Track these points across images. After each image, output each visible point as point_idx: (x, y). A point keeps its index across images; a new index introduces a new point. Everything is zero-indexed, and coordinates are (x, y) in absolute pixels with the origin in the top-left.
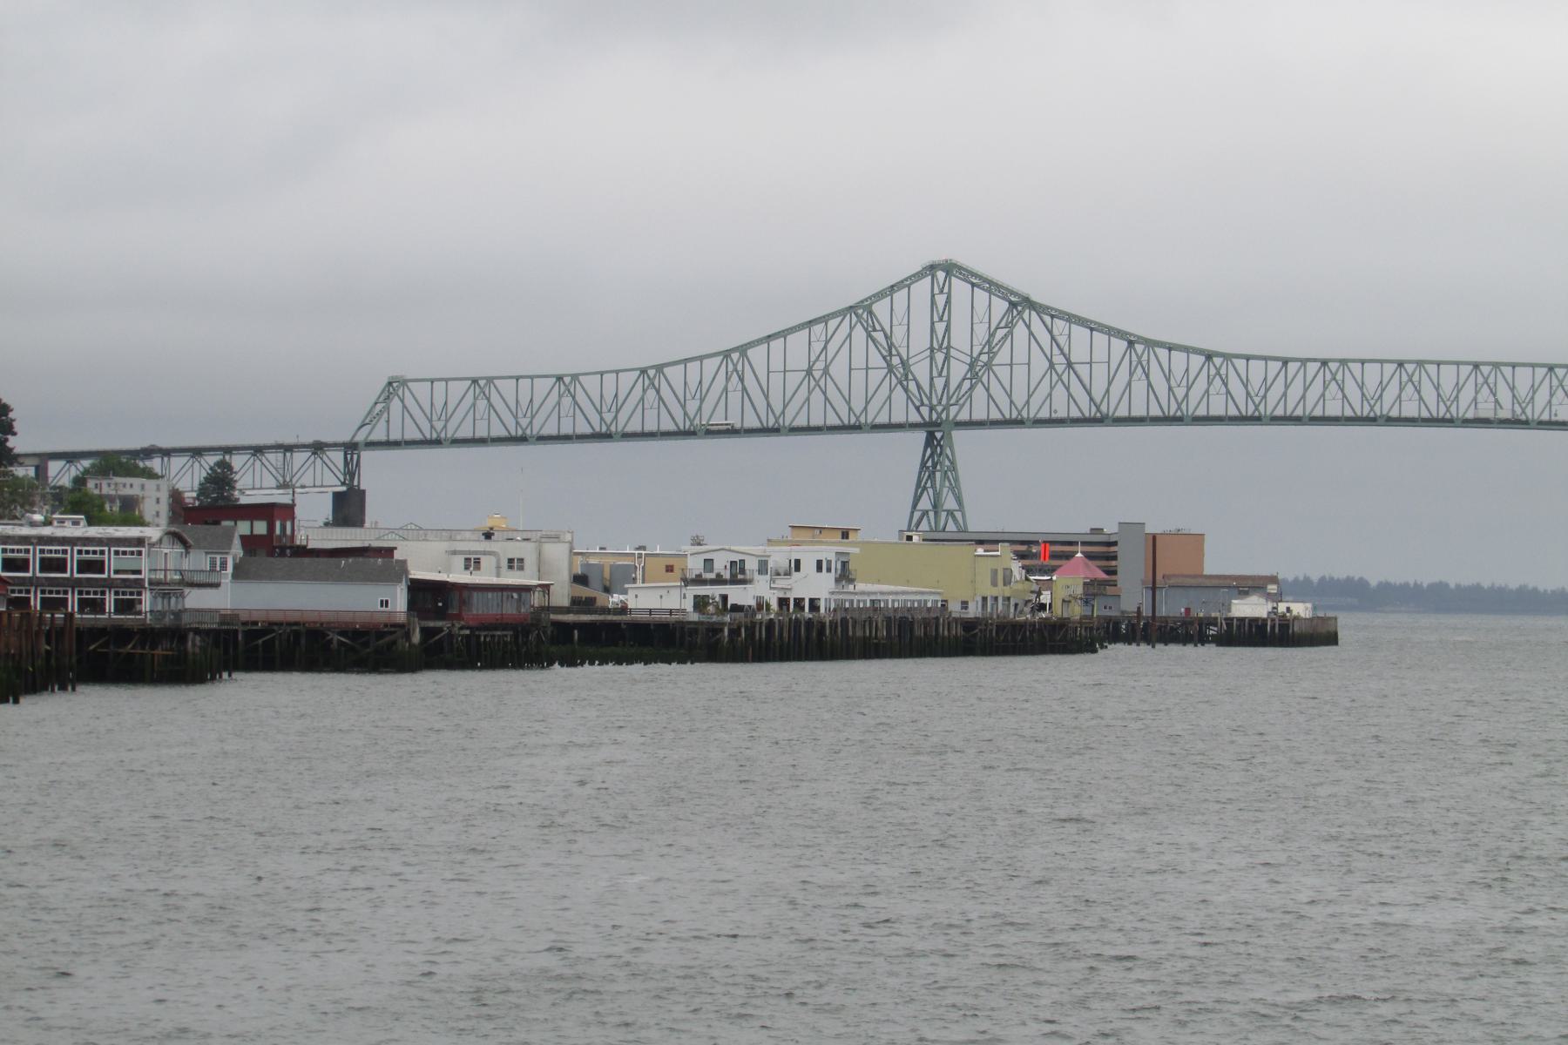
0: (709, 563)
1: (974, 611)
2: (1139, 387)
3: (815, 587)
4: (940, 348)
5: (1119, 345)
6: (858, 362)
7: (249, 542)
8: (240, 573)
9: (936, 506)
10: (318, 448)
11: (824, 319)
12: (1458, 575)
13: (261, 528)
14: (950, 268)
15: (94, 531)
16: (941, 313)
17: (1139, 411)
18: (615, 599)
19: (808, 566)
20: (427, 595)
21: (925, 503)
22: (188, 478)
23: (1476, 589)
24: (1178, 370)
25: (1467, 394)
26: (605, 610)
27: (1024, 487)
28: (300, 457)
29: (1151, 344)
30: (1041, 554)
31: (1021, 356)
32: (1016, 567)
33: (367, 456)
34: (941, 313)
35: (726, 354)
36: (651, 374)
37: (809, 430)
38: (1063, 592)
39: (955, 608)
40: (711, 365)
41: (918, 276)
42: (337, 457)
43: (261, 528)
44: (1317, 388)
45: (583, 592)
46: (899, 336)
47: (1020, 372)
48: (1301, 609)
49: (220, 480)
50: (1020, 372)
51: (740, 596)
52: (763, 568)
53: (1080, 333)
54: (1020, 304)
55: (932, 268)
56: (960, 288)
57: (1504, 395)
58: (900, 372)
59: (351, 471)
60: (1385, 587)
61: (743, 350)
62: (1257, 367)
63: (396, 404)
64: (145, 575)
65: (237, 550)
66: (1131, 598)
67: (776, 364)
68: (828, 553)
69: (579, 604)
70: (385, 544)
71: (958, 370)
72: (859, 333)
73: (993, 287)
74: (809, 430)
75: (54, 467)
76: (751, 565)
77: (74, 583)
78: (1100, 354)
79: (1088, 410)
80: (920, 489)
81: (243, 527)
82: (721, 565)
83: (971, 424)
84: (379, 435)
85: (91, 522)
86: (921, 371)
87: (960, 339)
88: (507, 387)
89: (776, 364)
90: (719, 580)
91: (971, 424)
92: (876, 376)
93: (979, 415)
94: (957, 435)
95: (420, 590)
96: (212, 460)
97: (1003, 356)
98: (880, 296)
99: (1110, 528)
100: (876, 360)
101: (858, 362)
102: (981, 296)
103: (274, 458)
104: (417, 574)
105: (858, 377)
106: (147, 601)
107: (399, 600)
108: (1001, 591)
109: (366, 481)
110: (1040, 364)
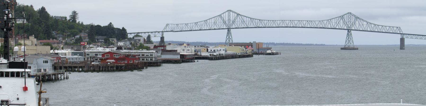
1: (240, 54)
2: (252, 24)
3: (223, 52)
4: (229, 20)
5: (250, 19)
6: (220, 21)
7: (162, 50)
8: (161, 54)
10: (159, 32)
11: (216, 17)
13: (163, 48)
14: (230, 11)
15: (148, 51)
16: (229, 16)
19: (222, 50)
20: (182, 56)
21: (228, 37)
22: (145, 36)
23: (287, 43)
24: (256, 22)
25: (289, 24)
26: (198, 55)
27: (241, 36)
28: (157, 33)
29: (253, 19)
30: (246, 45)
31: (238, 20)
33: (164, 33)
34: (229, 16)
36: (196, 23)
37: (205, 30)
38: (249, 51)
39: (238, 54)
40: (203, 22)
42: (161, 33)
43: (163, 48)
46: (224, 19)
47: (238, 22)
48: (274, 52)
49: (149, 37)
50: (238, 22)
51: (215, 54)
54: (238, 15)
56: (231, 13)
58: (225, 22)
59: (162, 35)
60: (277, 43)
61: (207, 20)
62: (265, 21)
64: (153, 56)
66: (255, 50)
67: (210, 22)
68: (224, 48)
69: (196, 54)
70: (176, 49)
71: (231, 22)
72: (220, 18)
73: (235, 13)
74: (205, 30)
76: (216, 50)
77: (145, 57)
79: (246, 27)
80: (227, 36)
81: (161, 48)
82: (213, 50)
84: (166, 30)
85: (147, 50)
86: (227, 22)
87: (231, 19)
88: (180, 25)
89: (210, 22)
92: (222, 23)
95: (181, 55)
96: (147, 35)
97: (236, 21)
98: (222, 14)
99: (252, 42)
100: (222, 21)
101: (220, 21)
104: (181, 53)
105: (220, 23)
106: (154, 59)
107: (179, 57)
108: (243, 52)
109: (164, 36)
110: (241, 21)
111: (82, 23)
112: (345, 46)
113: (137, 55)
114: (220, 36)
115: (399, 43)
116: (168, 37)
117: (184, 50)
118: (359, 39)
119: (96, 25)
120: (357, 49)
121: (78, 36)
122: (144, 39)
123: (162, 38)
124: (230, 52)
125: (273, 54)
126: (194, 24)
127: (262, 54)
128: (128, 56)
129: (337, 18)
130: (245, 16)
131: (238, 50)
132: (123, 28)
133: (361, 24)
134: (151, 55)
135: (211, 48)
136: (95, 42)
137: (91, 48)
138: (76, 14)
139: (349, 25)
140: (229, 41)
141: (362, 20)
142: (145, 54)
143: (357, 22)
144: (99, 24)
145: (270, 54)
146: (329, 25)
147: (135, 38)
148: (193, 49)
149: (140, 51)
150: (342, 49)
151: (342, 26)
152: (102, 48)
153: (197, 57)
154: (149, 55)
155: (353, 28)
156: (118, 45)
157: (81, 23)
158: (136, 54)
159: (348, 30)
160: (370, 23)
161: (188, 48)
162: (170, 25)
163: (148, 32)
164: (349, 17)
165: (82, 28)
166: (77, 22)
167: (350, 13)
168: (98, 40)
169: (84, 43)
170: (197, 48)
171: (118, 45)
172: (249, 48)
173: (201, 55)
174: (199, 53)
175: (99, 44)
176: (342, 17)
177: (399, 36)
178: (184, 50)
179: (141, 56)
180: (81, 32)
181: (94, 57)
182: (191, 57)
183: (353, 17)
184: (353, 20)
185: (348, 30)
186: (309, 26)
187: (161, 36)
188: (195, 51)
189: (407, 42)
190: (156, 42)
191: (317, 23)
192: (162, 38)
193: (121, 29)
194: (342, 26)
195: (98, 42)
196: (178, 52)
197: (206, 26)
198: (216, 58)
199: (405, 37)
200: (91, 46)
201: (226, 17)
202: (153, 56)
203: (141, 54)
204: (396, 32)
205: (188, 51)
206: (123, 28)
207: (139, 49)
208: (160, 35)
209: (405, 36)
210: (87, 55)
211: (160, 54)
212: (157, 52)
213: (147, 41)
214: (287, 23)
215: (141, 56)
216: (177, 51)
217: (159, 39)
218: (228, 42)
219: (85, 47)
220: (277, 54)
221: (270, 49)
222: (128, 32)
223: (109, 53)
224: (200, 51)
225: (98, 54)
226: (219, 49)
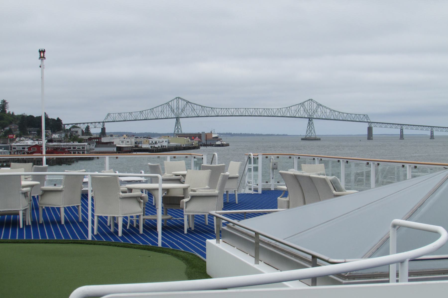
0: (152, 142)
1: (185, 146)
3: (165, 144)
4: (178, 108)
7: (96, 142)
8: (96, 147)
9: (178, 128)
10: (99, 123)
11: (163, 105)
12: (243, 132)
13: (98, 140)
14: (179, 98)
15: (79, 144)
16: (178, 103)
17: (203, 115)
18: (140, 145)
21: (176, 128)
22: (83, 127)
23: (246, 134)
24: (208, 110)
26: (139, 147)
27: (190, 126)
28: (97, 124)
29: (204, 107)
30: (192, 136)
31: (188, 109)
32: (190, 140)
34: (178, 103)
35: (151, 109)
36: (141, 112)
37: (161, 119)
38: (195, 142)
39: (182, 146)
40: (149, 111)
41: (175, 99)
42: (102, 124)
43: (98, 140)
44: (225, 112)
45: (136, 145)
46: (173, 106)
47: (188, 111)
48: (224, 143)
49: (88, 128)
52: (159, 142)
53: (195, 106)
54: (188, 102)
55: (177, 98)
57: (249, 112)
58: (173, 111)
59: (103, 125)
61: (153, 109)
62: (232, 110)
63: (109, 117)
64: (85, 149)
65: (95, 144)
66: (204, 141)
67: (157, 110)
68: (166, 140)
69: (136, 146)
70: (112, 141)
71: (180, 111)
72: (168, 106)
73: (184, 100)
74: (161, 119)
75: (66, 126)
76: (157, 142)
77: (77, 150)
78: (198, 108)
81: (95, 140)
82: (154, 142)
83: (182, 117)
84: (107, 121)
85: (79, 142)
86: (175, 111)
87: (180, 107)
88: (123, 114)
89: (157, 110)
90: (154, 144)
91: (182, 117)
92: (170, 112)
93: (183, 116)
94: (180, 119)
96: (86, 125)
97: (186, 109)
98: (170, 101)
99: (201, 132)
100: (170, 110)
102: (183, 101)
103: (94, 124)
104: (117, 145)
107: (115, 149)
108: (188, 143)
109: (105, 126)
110: (190, 110)
111: (13, 113)
112: (306, 136)
113: (66, 148)
114: (168, 127)
115: (366, 132)
116: (110, 128)
117: (123, 142)
118: (321, 128)
119: (28, 115)
120: (319, 139)
121: (7, 128)
122: (82, 130)
123: (103, 129)
124: (173, 144)
125: (222, 145)
126: (117, 115)
127: (211, 145)
128: (57, 149)
129: (297, 106)
130: (195, 104)
131: (183, 142)
132: (58, 118)
133: (323, 112)
134: (83, 148)
135: (155, 139)
136: (27, 134)
137: (22, 140)
138: (6, 103)
139: (311, 113)
140: (178, 131)
141: (325, 107)
142: (77, 147)
143: (319, 110)
144: (32, 115)
145: (219, 146)
146: (288, 113)
147: (73, 130)
148: (133, 140)
149: (71, 144)
150: (302, 139)
151: (302, 114)
152: (32, 141)
153: (137, 149)
154: (81, 147)
155: (315, 117)
156: (53, 137)
157: (11, 113)
158: (67, 147)
159: (309, 118)
160: (334, 111)
161: (128, 140)
162: (112, 115)
163: (88, 123)
164: (311, 104)
165: (13, 118)
166: (7, 112)
167: (312, 100)
168: (30, 132)
169: (12, 136)
170: (138, 140)
171: (53, 137)
172: (195, 139)
173: (141, 147)
174: (140, 145)
175: (31, 137)
176: (302, 104)
177: (366, 125)
178: (123, 142)
179: (72, 149)
180: (11, 123)
181: (21, 151)
182: (128, 149)
183: (315, 104)
184: (315, 108)
185: (309, 118)
186: (266, 115)
187: (101, 127)
188: (136, 143)
189: (376, 131)
190: (97, 134)
191: (275, 111)
192: (103, 129)
193: (56, 119)
194: (302, 114)
195: (31, 134)
196: (115, 144)
197: (152, 115)
198: (158, 150)
199: (373, 126)
200: (22, 139)
201: (174, 104)
202: (85, 149)
203: (72, 147)
204: (363, 120)
205: (128, 143)
206: (58, 118)
207: (69, 142)
208: (101, 126)
209: (373, 125)
210: (15, 148)
211: (94, 147)
212: (89, 144)
213: (85, 133)
214: (251, 112)
215: (72, 149)
216: (113, 142)
217: (99, 131)
218: (176, 132)
219: (12, 140)
220: (227, 145)
221: (220, 140)
222: (63, 123)
223: (36, 146)
224: (141, 143)
225: (26, 147)
226: (161, 140)
